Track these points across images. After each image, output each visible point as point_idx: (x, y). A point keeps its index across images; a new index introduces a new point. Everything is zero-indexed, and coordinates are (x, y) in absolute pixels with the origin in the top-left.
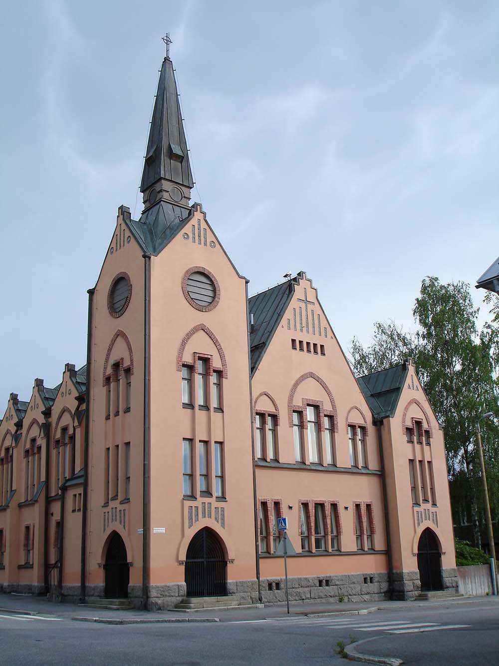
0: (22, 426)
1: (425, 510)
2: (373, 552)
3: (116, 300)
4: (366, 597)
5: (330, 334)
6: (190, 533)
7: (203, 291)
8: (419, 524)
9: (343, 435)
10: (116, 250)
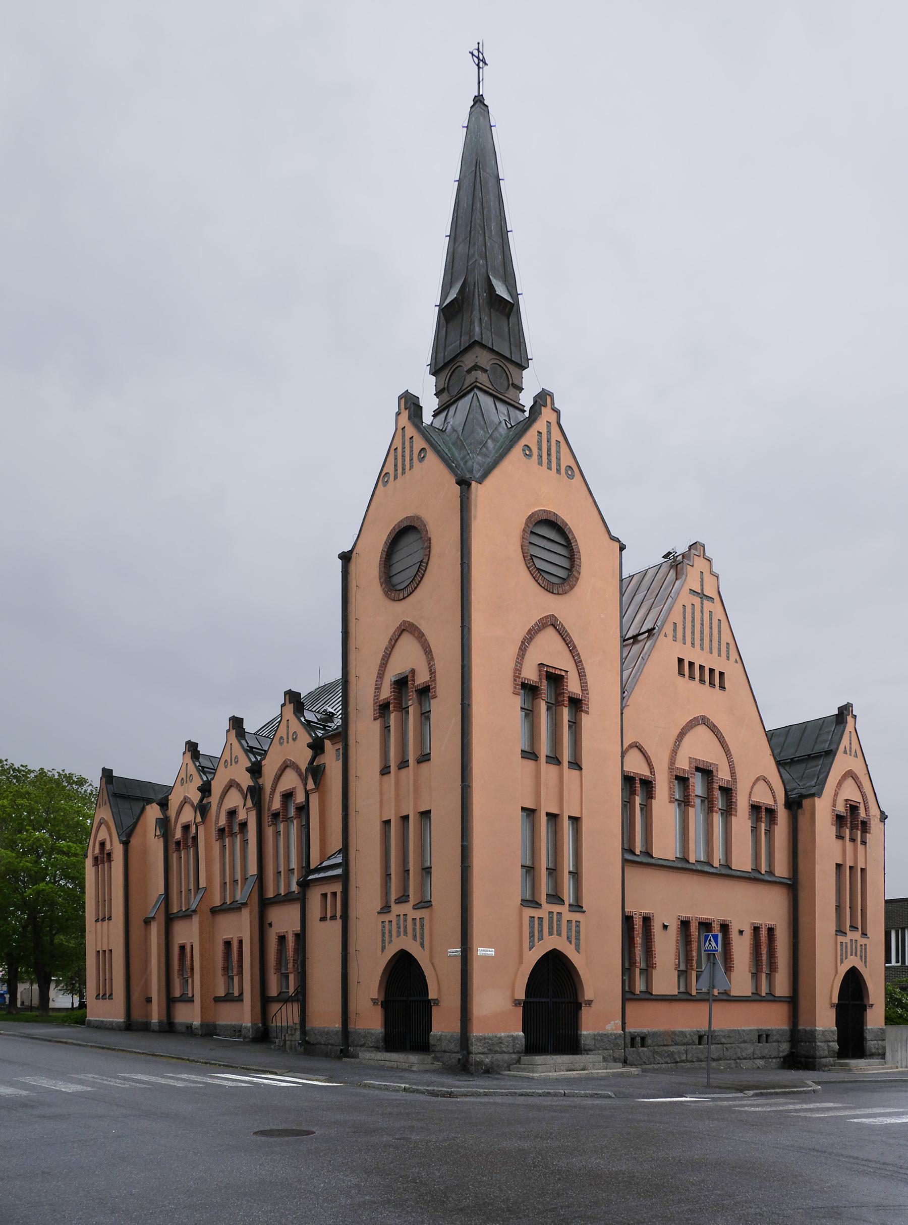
0: (209, 791)
1: (851, 940)
2: (759, 998)
3: (396, 568)
4: (761, 1062)
5: (734, 655)
6: (532, 957)
7: (554, 558)
8: (842, 962)
9: (742, 822)
10: (396, 478)
